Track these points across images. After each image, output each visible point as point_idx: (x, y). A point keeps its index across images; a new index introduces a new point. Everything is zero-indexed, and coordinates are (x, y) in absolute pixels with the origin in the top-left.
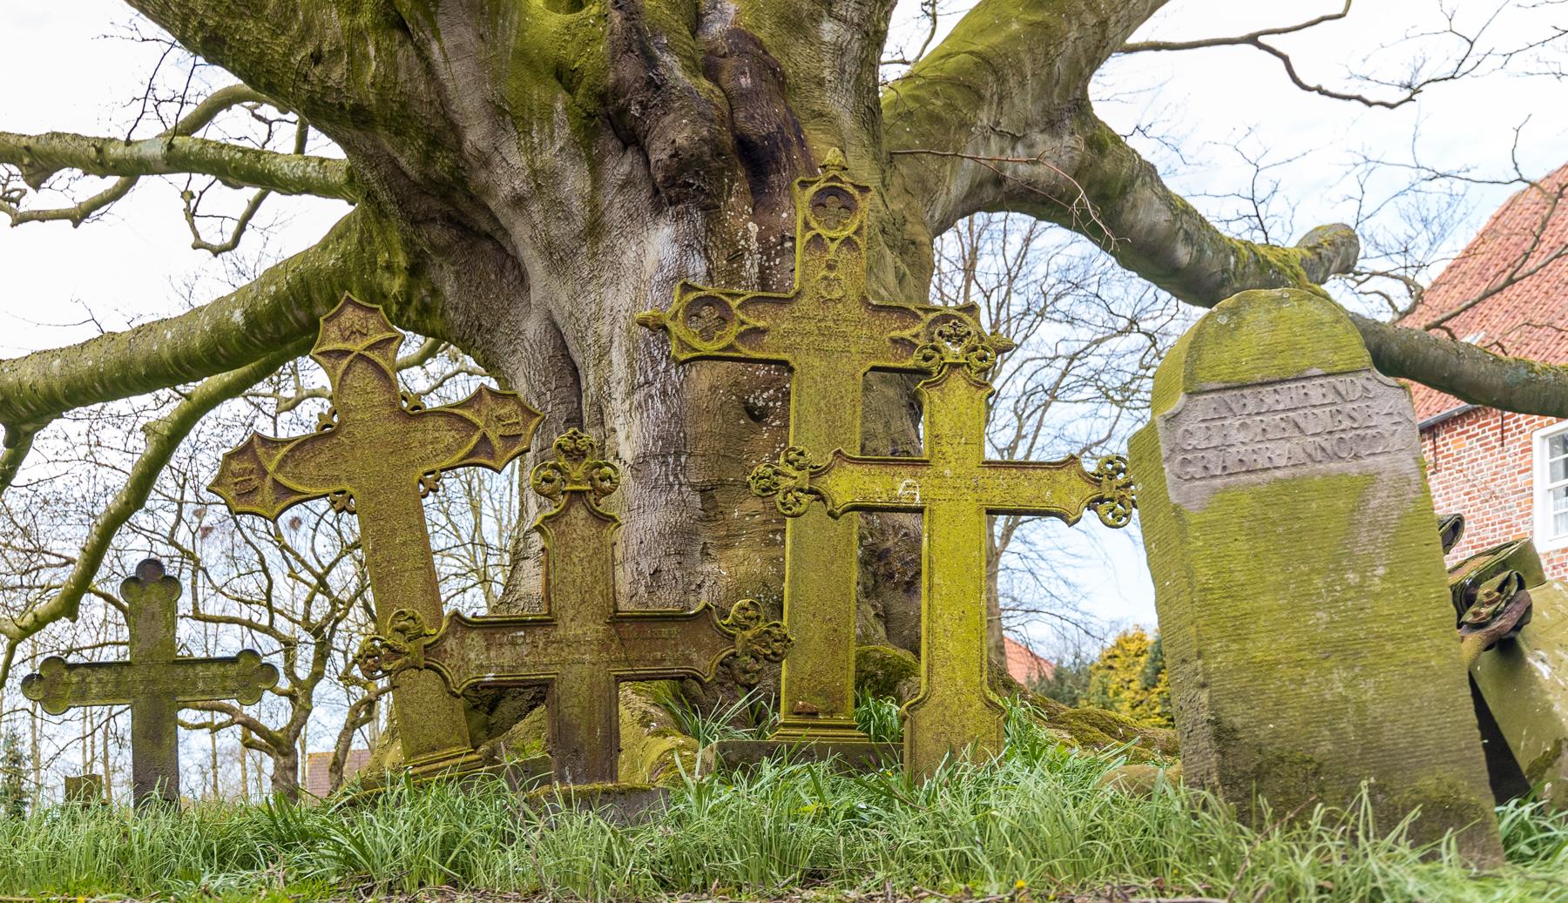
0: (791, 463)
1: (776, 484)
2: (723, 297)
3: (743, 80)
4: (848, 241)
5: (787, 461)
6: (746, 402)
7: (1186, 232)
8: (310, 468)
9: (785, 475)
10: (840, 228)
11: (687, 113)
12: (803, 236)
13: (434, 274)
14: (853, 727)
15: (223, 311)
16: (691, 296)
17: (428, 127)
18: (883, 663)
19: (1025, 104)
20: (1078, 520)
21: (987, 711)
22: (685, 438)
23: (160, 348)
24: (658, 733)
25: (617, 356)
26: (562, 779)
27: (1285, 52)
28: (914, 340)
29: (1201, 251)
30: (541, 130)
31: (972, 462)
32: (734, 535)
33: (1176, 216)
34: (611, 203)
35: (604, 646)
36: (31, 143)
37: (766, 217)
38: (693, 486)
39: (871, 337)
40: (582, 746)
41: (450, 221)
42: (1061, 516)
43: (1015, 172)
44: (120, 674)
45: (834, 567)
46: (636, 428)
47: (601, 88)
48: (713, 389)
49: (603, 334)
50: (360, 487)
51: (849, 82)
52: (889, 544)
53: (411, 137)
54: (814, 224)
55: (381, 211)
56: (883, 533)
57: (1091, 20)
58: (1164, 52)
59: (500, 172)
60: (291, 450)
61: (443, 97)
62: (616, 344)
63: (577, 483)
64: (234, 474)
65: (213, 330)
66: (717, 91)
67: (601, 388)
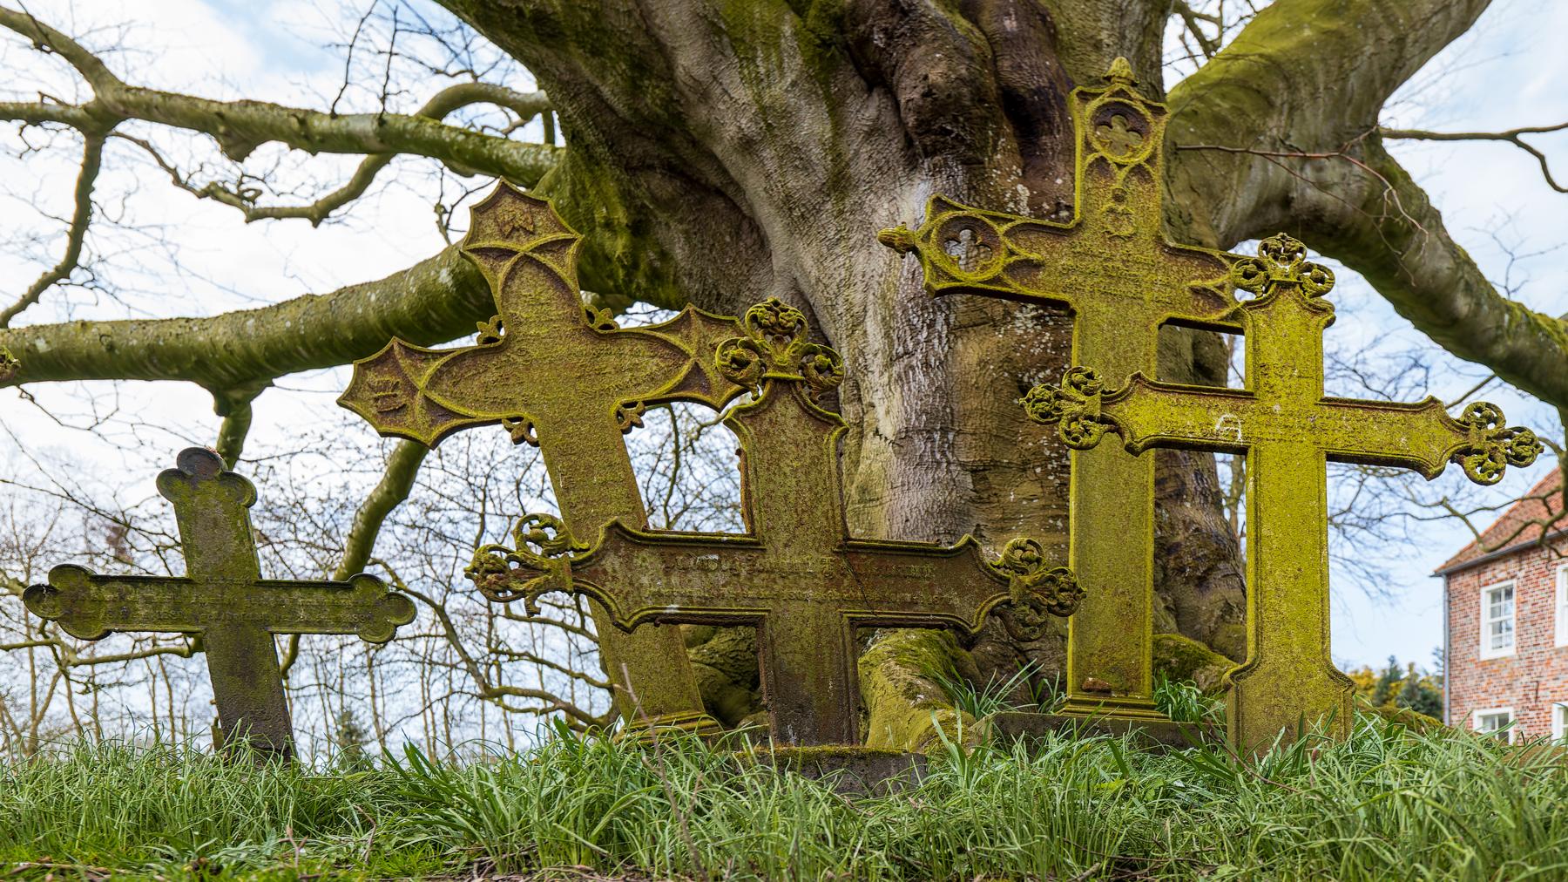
0: (1077, 386)
1: (1058, 409)
2: (987, 220)
3: (1007, 23)
4: (1138, 170)
5: (1072, 383)
6: (1020, 381)
7: (1467, 283)
8: (473, 387)
9: (1069, 399)
10: (1129, 154)
11: (942, 46)
12: (1084, 158)
13: (661, 234)
14: (1152, 708)
15: (428, 271)
16: (946, 215)
17: (630, 45)
18: (1177, 650)
19: (1315, 121)
20: (1440, 472)
21: (1331, 683)
22: (952, 414)
23: (365, 310)
24: (926, 706)
25: (872, 326)
26: (783, 738)
27: (1542, 151)
28: (1218, 292)
29: (1479, 305)
30: (767, 59)
31: (1309, 399)
32: (1011, 519)
33: (1458, 264)
34: (857, 153)
35: (832, 580)
36: (224, 110)
37: (1038, 181)
38: (963, 465)
39: (1168, 285)
40: (809, 700)
41: (674, 170)
42: (1417, 467)
43: (1303, 195)
44: (178, 593)
45: (1127, 537)
46: (896, 401)
47: (836, 9)
48: (983, 363)
49: (855, 302)
50: (542, 415)
51: (1129, 50)
52: (1179, 538)
53: (611, 59)
54: (1096, 145)
55: (591, 157)
56: (1172, 527)
57: (1389, 35)
58: (1427, 142)
59: (722, 107)
60: (445, 365)
61: (643, 7)
62: (870, 313)
63: (782, 369)
64: (372, 388)
65: (420, 291)
66: (977, 33)
67: (856, 360)
